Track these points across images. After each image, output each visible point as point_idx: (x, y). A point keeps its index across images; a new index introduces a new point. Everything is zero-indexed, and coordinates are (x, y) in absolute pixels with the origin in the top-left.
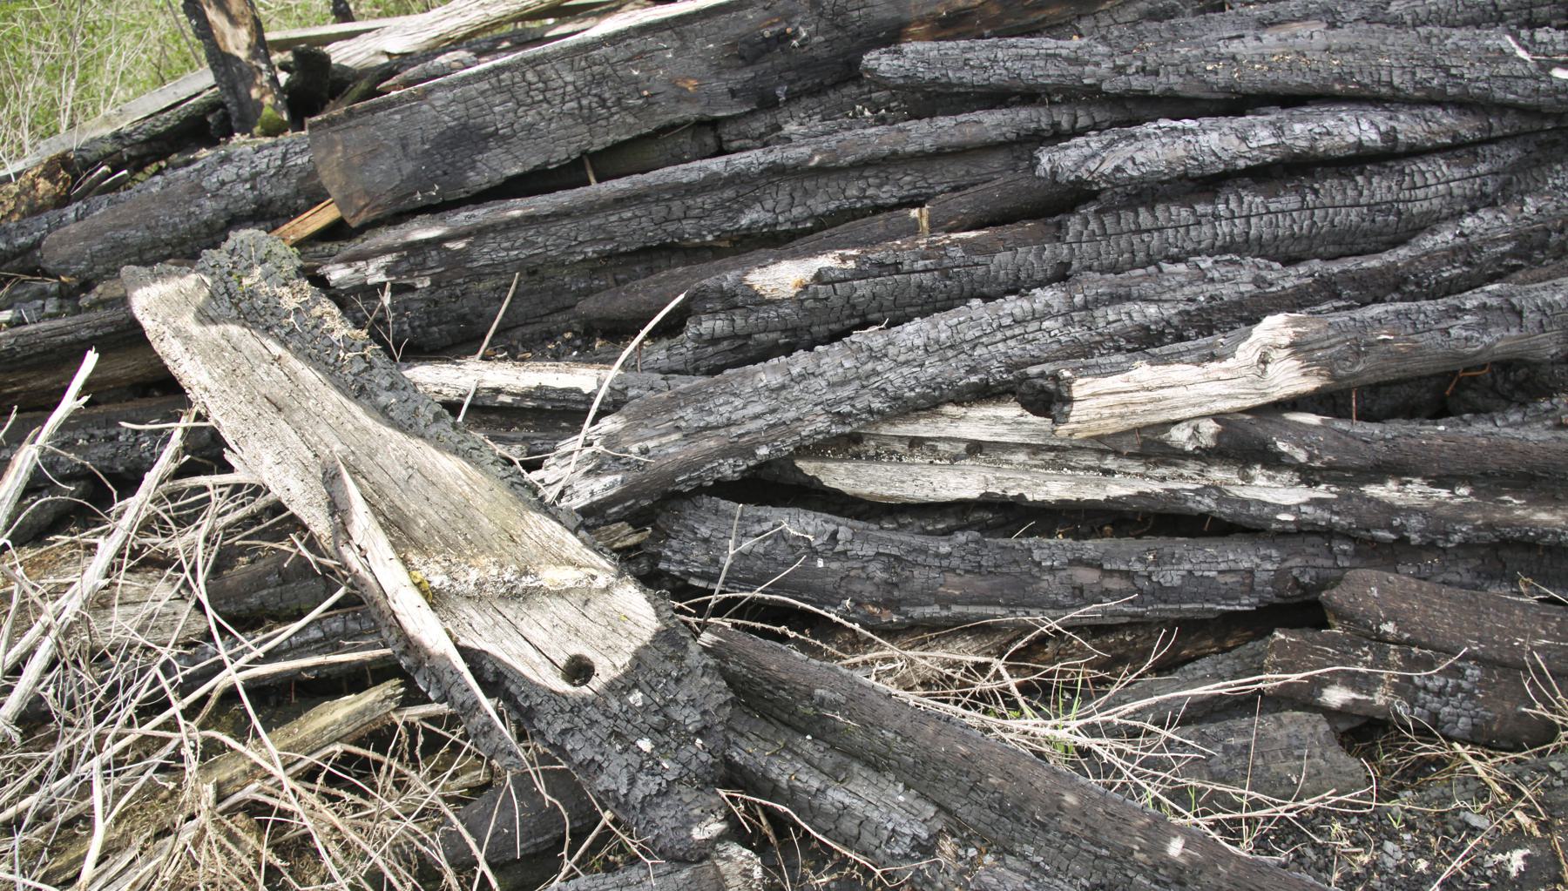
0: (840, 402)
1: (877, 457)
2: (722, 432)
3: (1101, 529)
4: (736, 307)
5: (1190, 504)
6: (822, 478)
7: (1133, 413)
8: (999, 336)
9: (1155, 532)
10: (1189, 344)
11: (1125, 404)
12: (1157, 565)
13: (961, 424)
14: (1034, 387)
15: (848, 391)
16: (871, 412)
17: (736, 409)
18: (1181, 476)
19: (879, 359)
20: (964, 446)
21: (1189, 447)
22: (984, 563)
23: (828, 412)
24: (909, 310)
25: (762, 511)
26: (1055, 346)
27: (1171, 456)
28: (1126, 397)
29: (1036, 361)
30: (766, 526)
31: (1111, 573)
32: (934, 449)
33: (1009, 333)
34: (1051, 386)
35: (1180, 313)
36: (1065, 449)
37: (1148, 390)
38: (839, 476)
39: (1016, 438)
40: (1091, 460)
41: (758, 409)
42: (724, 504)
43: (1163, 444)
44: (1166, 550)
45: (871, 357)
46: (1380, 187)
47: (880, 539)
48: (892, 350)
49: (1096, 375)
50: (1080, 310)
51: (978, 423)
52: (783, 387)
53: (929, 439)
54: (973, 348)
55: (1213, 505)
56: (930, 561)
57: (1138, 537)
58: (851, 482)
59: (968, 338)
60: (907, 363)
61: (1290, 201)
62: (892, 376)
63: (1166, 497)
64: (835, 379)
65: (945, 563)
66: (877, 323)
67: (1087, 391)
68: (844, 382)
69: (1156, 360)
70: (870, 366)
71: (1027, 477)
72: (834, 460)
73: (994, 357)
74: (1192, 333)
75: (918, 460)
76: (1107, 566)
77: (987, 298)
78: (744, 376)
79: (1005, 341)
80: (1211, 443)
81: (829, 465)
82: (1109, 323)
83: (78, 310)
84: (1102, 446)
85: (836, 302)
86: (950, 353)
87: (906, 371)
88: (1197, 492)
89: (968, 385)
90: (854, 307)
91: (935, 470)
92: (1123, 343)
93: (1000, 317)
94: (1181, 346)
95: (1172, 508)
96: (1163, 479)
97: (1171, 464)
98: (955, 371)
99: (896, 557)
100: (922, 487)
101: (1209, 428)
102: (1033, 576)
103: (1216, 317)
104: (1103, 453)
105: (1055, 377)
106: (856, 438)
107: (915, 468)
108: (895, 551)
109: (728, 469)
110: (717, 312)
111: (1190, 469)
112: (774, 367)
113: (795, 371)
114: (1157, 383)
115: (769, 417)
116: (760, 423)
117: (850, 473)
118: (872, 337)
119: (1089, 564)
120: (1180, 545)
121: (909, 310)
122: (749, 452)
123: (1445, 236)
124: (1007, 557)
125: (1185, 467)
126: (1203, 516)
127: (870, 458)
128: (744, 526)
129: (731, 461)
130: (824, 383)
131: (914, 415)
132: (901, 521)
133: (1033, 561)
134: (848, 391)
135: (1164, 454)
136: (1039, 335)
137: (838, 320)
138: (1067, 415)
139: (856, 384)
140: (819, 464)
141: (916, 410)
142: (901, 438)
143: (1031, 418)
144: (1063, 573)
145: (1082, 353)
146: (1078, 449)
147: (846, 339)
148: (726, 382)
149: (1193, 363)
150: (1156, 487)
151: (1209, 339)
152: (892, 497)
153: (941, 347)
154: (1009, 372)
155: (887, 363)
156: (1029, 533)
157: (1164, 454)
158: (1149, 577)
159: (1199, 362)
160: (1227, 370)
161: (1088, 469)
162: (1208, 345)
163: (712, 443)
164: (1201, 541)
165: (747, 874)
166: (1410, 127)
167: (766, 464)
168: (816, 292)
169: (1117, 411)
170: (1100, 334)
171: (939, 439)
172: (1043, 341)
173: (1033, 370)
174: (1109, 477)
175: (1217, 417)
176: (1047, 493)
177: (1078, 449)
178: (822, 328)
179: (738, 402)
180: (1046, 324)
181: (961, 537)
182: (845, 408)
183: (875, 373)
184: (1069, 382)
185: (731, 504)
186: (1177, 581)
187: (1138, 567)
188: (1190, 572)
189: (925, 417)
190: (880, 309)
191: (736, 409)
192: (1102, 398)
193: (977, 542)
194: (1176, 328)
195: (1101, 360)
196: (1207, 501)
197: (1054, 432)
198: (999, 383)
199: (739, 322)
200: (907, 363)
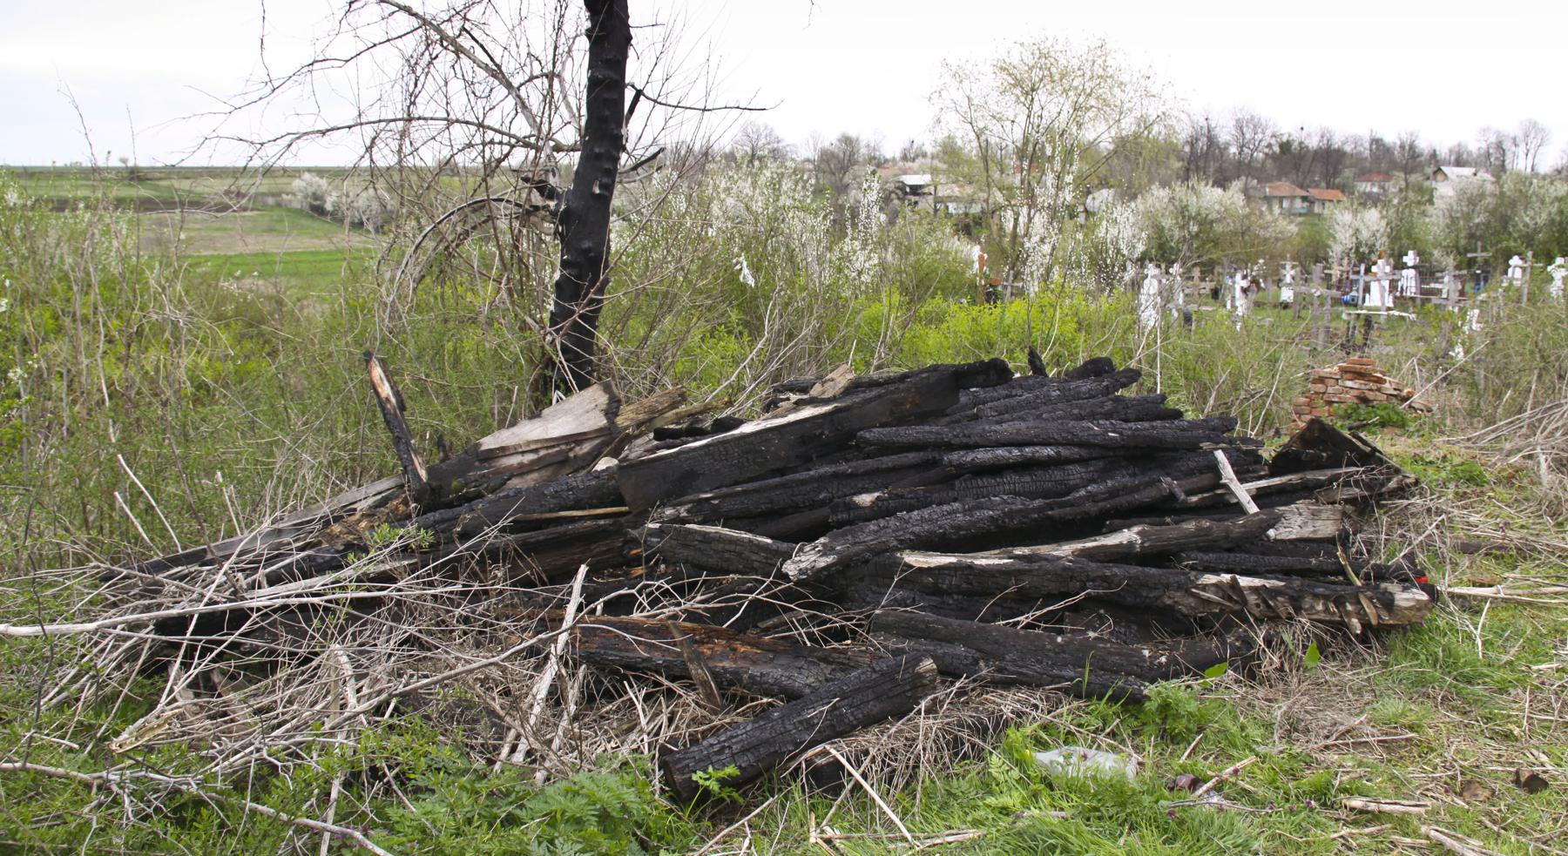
46: (1057, 474)
61: (1028, 479)
83: (1053, 157)
123: (1083, 492)
165: (1560, 266)
166: (1065, 452)
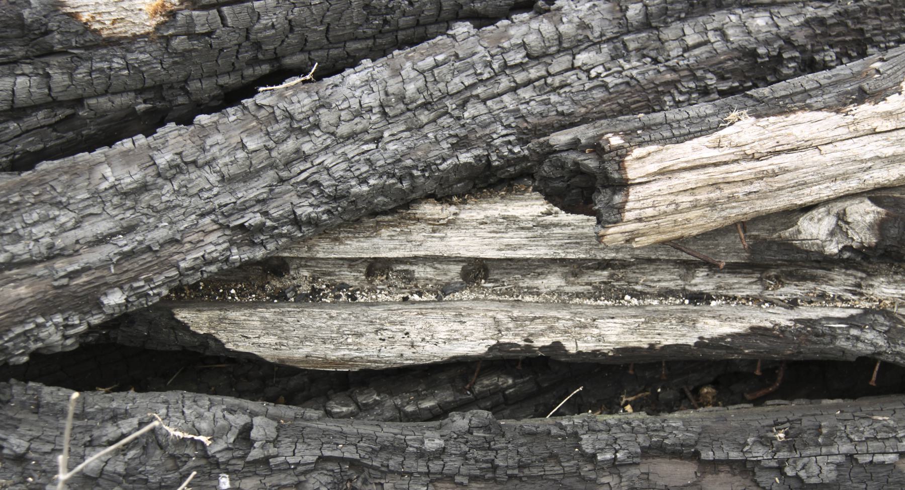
0: (243, 209)
1: (314, 297)
2: (40, 270)
3: (696, 391)
4: (51, 53)
5: (842, 343)
6: (222, 336)
7: (731, 198)
8: (504, 82)
9: (787, 393)
10: (821, 76)
11: (716, 185)
12: (793, 448)
13: (449, 233)
14: (563, 166)
15: (255, 190)
16: (296, 221)
17: (63, 229)
18: (823, 296)
19: (306, 132)
20: (456, 269)
21: (833, 248)
22: (499, 462)
23: (223, 227)
24: (352, 46)
25: (119, 401)
26: (598, 94)
27: (807, 264)
28: (717, 173)
29: (567, 122)
30: (125, 426)
31: (715, 465)
32: (408, 277)
33: (520, 77)
34: (591, 163)
35: (807, 23)
36: (624, 265)
37: (753, 158)
38: (250, 331)
39: (542, 251)
40: (669, 279)
41: (103, 226)
42: (49, 393)
43: (787, 246)
44: (806, 422)
45: (291, 130)
47: (325, 433)
48: (326, 117)
49: (665, 141)
50: (638, 30)
51: (477, 230)
52: (144, 187)
53: (399, 261)
54: (463, 106)
55: (881, 342)
56: (411, 464)
57: (758, 402)
58: (272, 340)
59: (452, 88)
60: (352, 136)
62: (328, 159)
63: (798, 333)
64: (233, 170)
65: (435, 466)
66: (299, 71)
67: (652, 167)
68: (249, 175)
69: (764, 109)
70: (290, 145)
71: (564, 314)
72: (241, 305)
73: (497, 119)
74: (830, 55)
75: (382, 297)
76: (707, 455)
77: (481, 20)
78: (74, 171)
79: (514, 90)
80: (871, 239)
81: (233, 315)
82: (687, 49)
84: (684, 256)
85: (227, 38)
86: (424, 117)
87: (351, 150)
88: (851, 321)
89: (457, 168)
90: (258, 45)
91: (411, 312)
92: (711, 80)
93: (504, 51)
94: (808, 80)
95: (810, 350)
96: (793, 304)
97: (804, 278)
98: (434, 146)
99: (353, 463)
100: (392, 341)
101: (864, 214)
102: (583, 479)
103: (870, 24)
104: (689, 266)
105: (597, 148)
106: (276, 267)
107: (378, 312)
108: (350, 453)
109: (53, 333)
110: (16, 62)
111: (838, 283)
112: (125, 154)
113: (163, 159)
114: (769, 145)
115: (121, 240)
116: (106, 251)
117: (268, 326)
118: (293, 96)
119: (677, 453)
120: (830, 413)
121: (352, 46)
122: (90, 300)
124: (539, 450)
125: (829, 281)
126: (866, 362)
127: (302, 299)
128: (88, 429)
129: (58, 319)
130: (214, 178)
131: (371, 222)
132: (362, 399)
133: (583, 454)
134: (255, 190)
135: (791, 262)
136: (571, 77)
137: (233, 69)
138: (621, 209)
139: (270, 176)
140: (215, 313)
141: (374, 214)
142: (352, 263)
143: (564, 217)
144: (635, 471)
145: (643, 104)
146: (646, 262)
147: (248, 102)
148: (41, 183)
149: (828, 108)
150: (783, 318)
151: (856, 65)
152: (343, 361)
153: (409, 106)
154: (522, 142)
155: (319, 138)
156: (576, 407)
157: (791, 262)
158: (780, 469)
159: (838, 107)
160: (889, 115)
161: (665, 294)
162: (854, 76)
163: (23, 291)
164: (866, 404)
167: (123, 319)
168: (191, 22)
169: (703, 196)
170: (673, 69)
171: (415, 260)
172: (577, 86)
173: (560, 138)
174: (701, 306)
175: (876, 195)
176: (600, 338)
177: (646, 262)
178: (207, 84)
179: (65, 217)
180: (582, 58)
181: (460, 421)
182: (253, 218)
183: (300, 156)
184: (620, 154)
185: (63, 392)
186: (829, 474)
187: (760, 453)
188: (850, 457)
189: (389, 225)
190: (303, 47)
191: (63, 229)
192: (677, 178)
193: (486, 428)
194: (802, 49)
195: (672, 114)
196: (870, 335)
197: (600, 238)
198: (508, 162)
199: (59, 78)
200: (352, 136)
